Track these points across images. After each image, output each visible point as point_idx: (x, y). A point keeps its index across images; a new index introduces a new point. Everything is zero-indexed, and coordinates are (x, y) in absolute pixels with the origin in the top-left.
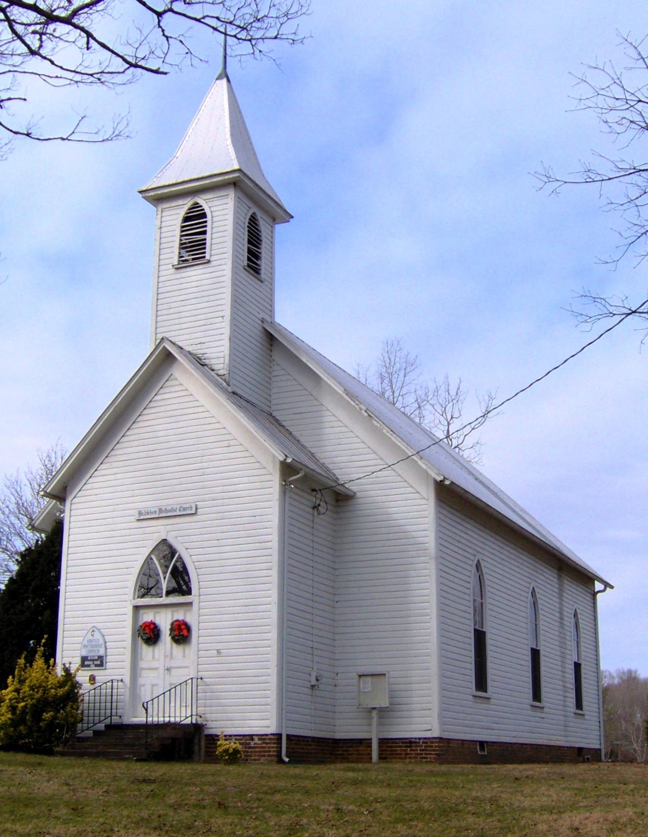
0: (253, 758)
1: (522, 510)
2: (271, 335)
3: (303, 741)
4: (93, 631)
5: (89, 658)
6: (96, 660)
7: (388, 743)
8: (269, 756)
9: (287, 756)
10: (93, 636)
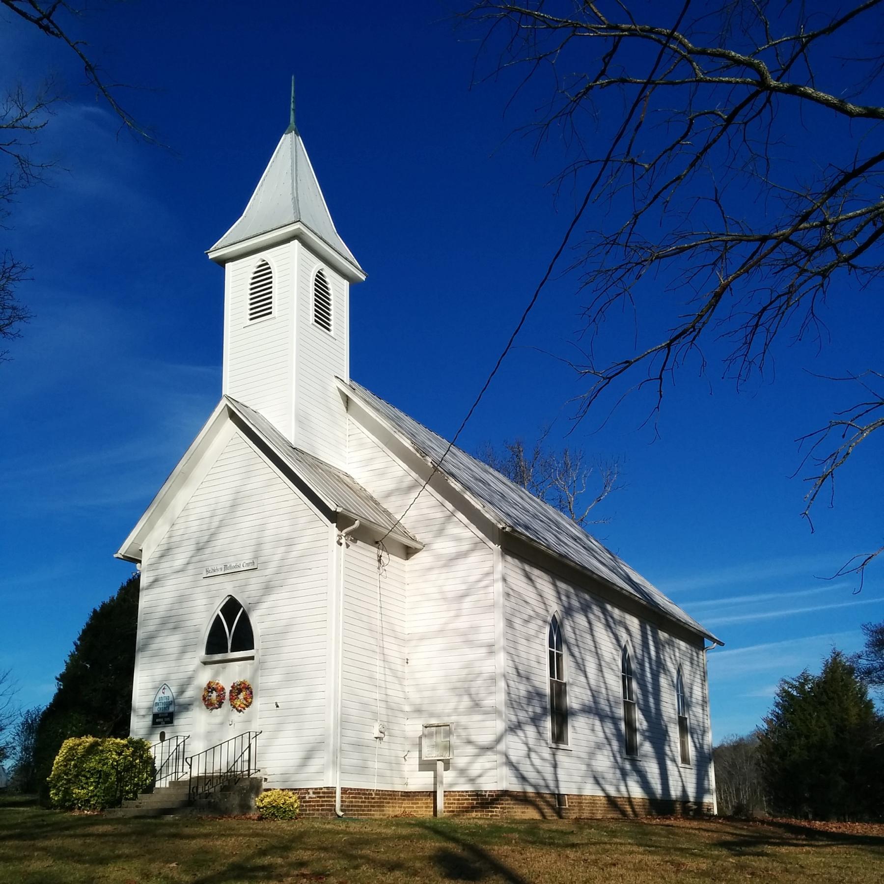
0: (308, 812)
1: (292, 159)
2: (347, 396)
3: (364, 794)
4: (164, 689)
5: (160, 716)
6: (167, 717)
7: (455, 796)
8: (322, 810)
9: (342, 810)
10: (163, 693)
